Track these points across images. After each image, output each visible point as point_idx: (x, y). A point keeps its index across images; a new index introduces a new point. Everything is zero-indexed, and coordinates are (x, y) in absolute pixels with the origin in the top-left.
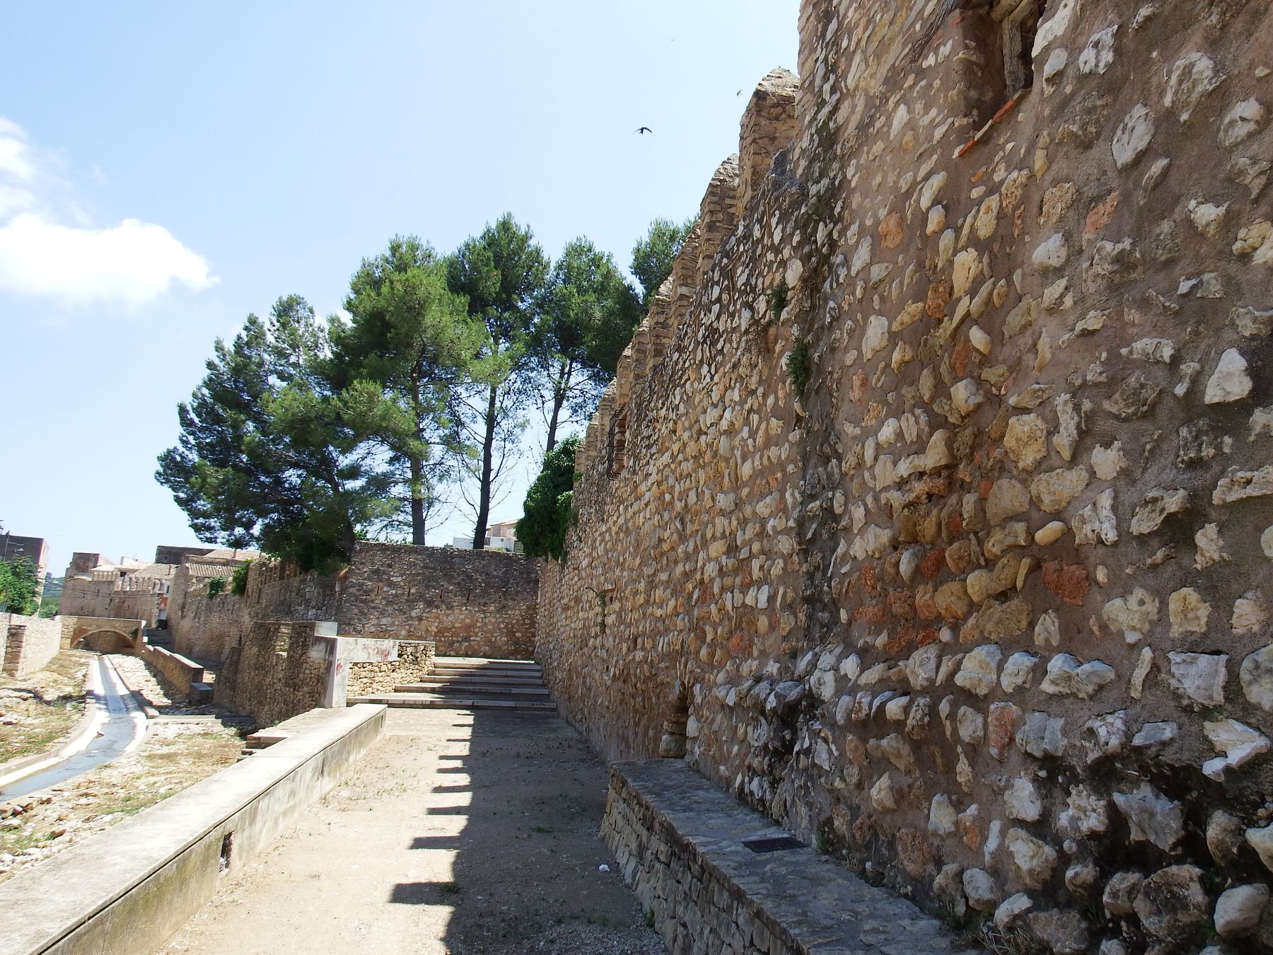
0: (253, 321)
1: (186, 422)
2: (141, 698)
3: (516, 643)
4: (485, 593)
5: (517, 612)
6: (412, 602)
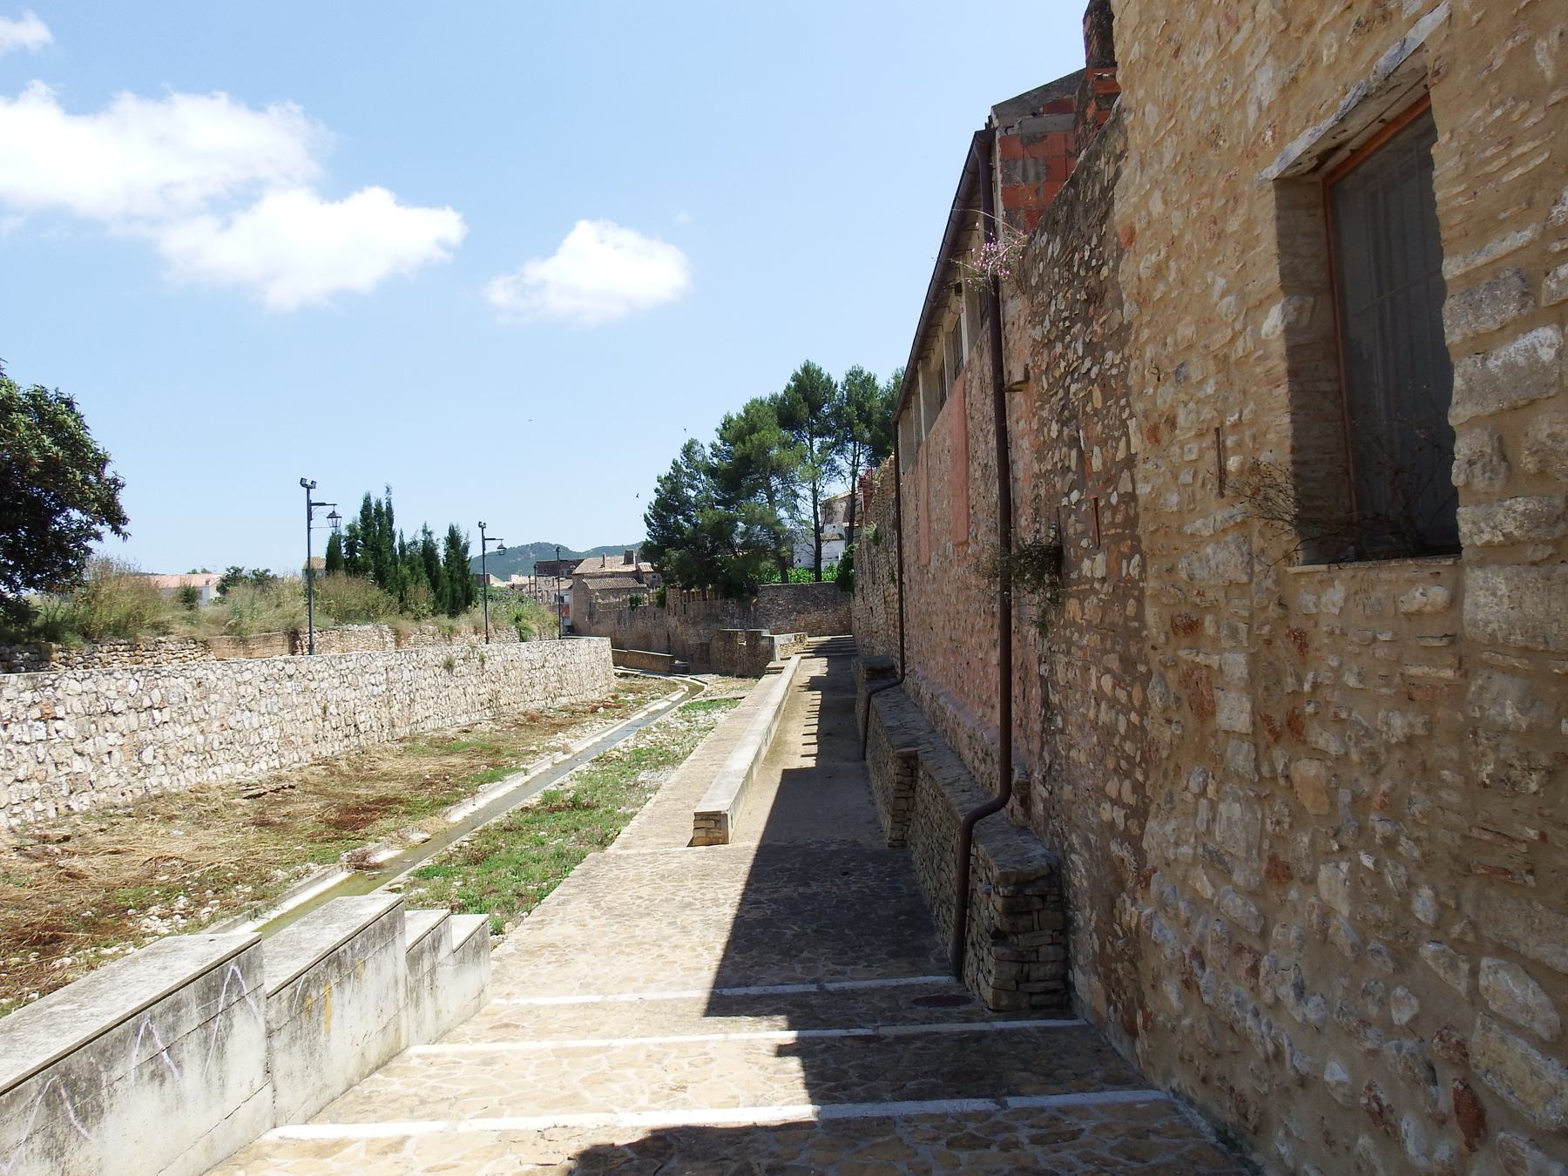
0: (675, 463)
1: (649, 525)
2: (739, 669)
5: (842, 611)
6: (790, 612)
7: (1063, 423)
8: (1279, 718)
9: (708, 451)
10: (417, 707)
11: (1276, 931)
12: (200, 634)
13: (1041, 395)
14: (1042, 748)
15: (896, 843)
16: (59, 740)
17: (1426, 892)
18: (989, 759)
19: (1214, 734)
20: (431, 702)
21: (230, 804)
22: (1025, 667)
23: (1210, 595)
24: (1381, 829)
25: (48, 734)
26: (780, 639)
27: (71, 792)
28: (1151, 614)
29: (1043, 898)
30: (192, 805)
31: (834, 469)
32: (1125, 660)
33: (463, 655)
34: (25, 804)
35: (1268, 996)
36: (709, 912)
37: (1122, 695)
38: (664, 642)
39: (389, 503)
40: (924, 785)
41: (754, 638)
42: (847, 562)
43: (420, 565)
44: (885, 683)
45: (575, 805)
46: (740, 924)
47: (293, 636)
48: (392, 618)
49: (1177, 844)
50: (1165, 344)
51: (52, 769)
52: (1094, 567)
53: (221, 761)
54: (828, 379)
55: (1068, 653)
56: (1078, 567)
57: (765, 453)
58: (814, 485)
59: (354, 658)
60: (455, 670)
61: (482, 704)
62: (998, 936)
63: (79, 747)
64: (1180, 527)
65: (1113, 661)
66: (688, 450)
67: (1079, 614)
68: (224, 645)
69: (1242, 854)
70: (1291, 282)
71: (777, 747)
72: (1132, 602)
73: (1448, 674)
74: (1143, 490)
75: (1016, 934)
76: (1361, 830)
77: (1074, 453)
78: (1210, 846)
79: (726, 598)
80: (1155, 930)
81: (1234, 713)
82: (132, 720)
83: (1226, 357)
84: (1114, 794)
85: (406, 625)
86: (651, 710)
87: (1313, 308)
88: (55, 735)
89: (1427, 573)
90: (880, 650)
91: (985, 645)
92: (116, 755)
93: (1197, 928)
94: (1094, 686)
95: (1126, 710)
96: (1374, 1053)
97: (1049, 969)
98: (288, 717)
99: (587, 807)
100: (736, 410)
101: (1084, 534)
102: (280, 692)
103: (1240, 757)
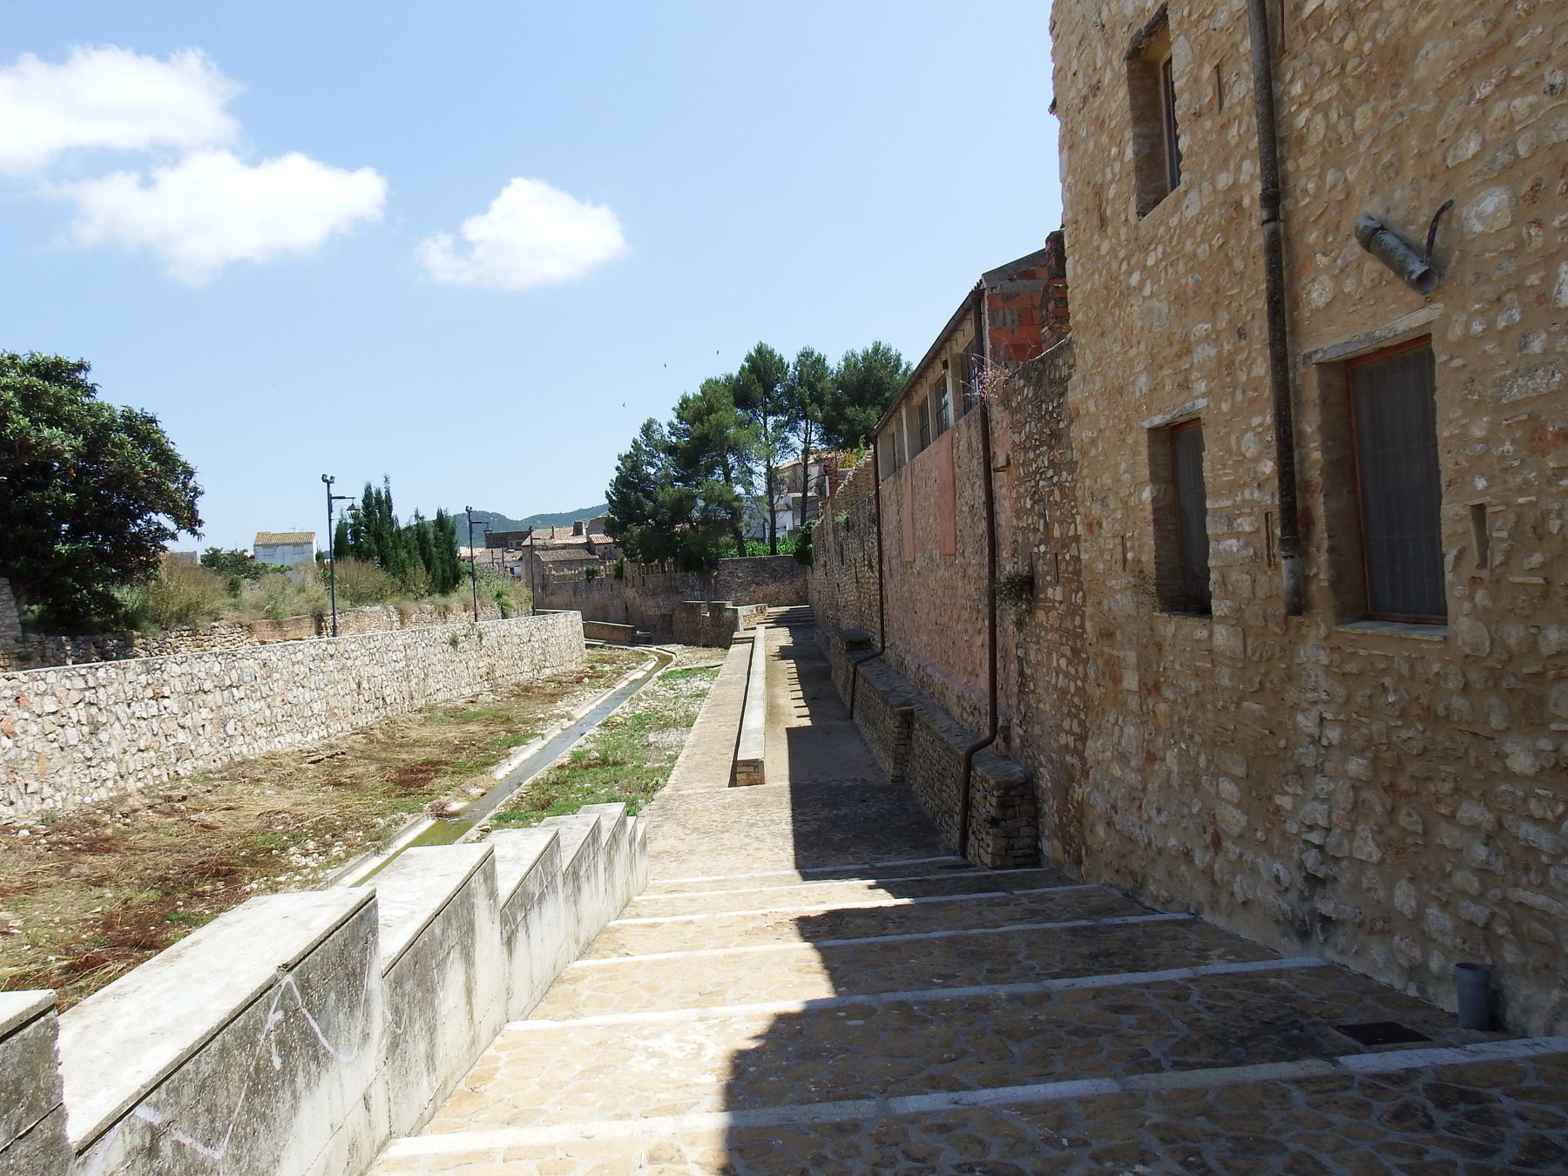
2: (702, 640)
4: (783, 576)
5: (799, 583)
6: (749, 584)
7: (1035, 502)
8: (1150, 683)
9: (666, 430)
10: (430, 681)
11: (1149, 785)
12: (246, 620)
13: (1018, 478)
14: (1019, 703)
15: (897, 779)
16: (167, 715)
17: (1203, 756)
18: (976, 713)
19: (1122, 692)
20: (441, 676)
21: (301, 769)
22: (1006, 651)
23: (1119, 620)
24: (1188, 731)
25: (160, 711)
26: (743, 611)
27: (178, 760)
28: (1088, 625)
29: (1022, 797)
30: (270, 770)
31: (786, 446)
32: (1073, 650)
33: (464, 632)
34: (145, 770)
35: (1145, 817)
36: (771, 828)
37: (1072, 670)
38: (622, 614)
39: (388, 492)
40: (921, 735)
41: (719, 609)
43: (415, 548)
45: (604, 762)
47: (319, 619)
48: (396, 599)
49: (1103, 752)
50: (1096, 482)
52: (1055, 593)
53: (284, 732)
54: (781, 359)
55: (1038, 643)
57: (722, 432)
58: (769, 462)
59: (380, 637)
61: (481, 677)
62: (994, 822)
63: (181, 721)
64: (1104, 582)
65: (1067, 650)
66: (647, 429)
67: (1045, 619)
68: (264, 630)
69: (1135, 752)
70: (1154, 477)
71: (772, 713)
72: (1078, 617)
73: (1209, 665)
74: (1084, 557)
75: (1005, 820)
76: (1183, 733)
77: (1042, 522)
78: (1120, 750)
79: (687, 571)
80: (1092, 799)
81: (1131, 681)
82: (216, 698)
83: (1126, 502)
84: (1068, 728)
85: (409, 606)
86: (631, 679)
87: (1165, 491)
88: (164, 712)
89: (1201, 624)
90: (848, 623)
91: (971, 630)
92: (208, 728)
93: (1113, 794)
94: (1055, 664)
95: (1075, 679)
96: (1185, 828)
97: (1027, 841)
99: (616, 764)
100: (694, 390)
101: (1048, 573)
102: (325, 669)
103: (1133, 703)
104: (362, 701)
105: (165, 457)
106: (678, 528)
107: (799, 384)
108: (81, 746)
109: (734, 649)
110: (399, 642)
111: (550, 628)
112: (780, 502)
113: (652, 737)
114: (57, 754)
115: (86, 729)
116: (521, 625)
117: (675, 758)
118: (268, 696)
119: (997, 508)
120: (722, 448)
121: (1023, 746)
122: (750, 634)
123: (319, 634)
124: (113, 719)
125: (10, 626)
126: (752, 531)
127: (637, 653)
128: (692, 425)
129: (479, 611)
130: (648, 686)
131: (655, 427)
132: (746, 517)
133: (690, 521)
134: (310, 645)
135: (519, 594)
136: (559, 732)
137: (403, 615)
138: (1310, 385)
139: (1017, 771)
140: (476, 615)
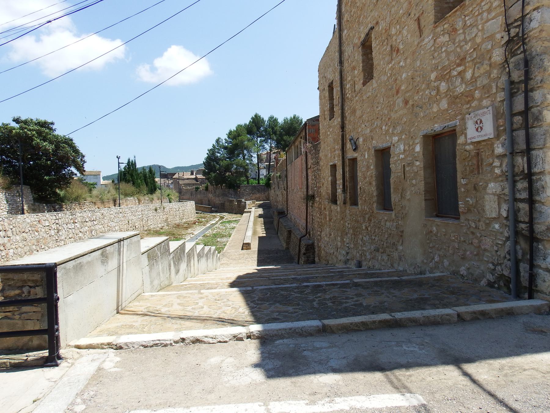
3: (267, 198)
4: (261, 191)
5: (266, 194)
6: (250, 194)
9: (224, 141)
10: (149, 222)
12: (94, 201)
20: (152, 220)
29: (311, 248)
33: (159, 207)
38: (207, 202)
39: (135, 161)
40: (292, 236)
41: (240, 202)
42: (269, 179)
44: (282, 216)
46: (258, 260)
47: (115, 201)
48: (137, 195)
51: (76, 235)
52: (317, 199)
54: (263, 119)
56: (316, 199)
57: (242, 143)
58: (258, 153)
60: (158, 211)
61: (164, 221)
66: (218, 141)
68: (99, 204)
71: (255, 232)
74: (322, 191)
85: (142, 198)
86: (211, 223)
90: (280, 207)
92: (87, 232)
97: (312, 258)
98: (121, 224)
100: (234, 128)
104: (129, 227)
105: (76, 151)
106: (227, 174)
107: (269, 127)
108: (55, 236)
109: (244, 215)
110: (140, 209)
111: (185, 206)
112: (261, 165)
113: (219, 240)
114: (49, 238)
115: (56, 231)
116: (175, 205)
117: (225, 245)
118: (103, 224)
119: (308, 178)
120: (242, 147)
121: (312, 236)
122: (250, 210)
123: (115, 206)
124: (63, 229)
125: (30, 200)
126: (252, 176)
127: (213, 215)
128: (233, 140)
129: (162, 200)
130: (217, 225)
131: (220, 140)
132: (250, 171)
133: (231, 172)
134: (114, 210)
135: (175, 195)
136: (190, 238)
137: (139, 201)
138: (347, 162)
139: (311, 242)
140: (161, 202)
